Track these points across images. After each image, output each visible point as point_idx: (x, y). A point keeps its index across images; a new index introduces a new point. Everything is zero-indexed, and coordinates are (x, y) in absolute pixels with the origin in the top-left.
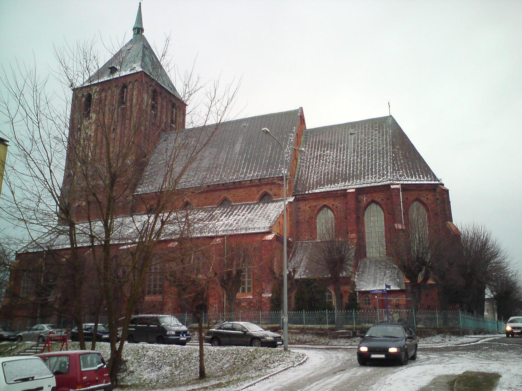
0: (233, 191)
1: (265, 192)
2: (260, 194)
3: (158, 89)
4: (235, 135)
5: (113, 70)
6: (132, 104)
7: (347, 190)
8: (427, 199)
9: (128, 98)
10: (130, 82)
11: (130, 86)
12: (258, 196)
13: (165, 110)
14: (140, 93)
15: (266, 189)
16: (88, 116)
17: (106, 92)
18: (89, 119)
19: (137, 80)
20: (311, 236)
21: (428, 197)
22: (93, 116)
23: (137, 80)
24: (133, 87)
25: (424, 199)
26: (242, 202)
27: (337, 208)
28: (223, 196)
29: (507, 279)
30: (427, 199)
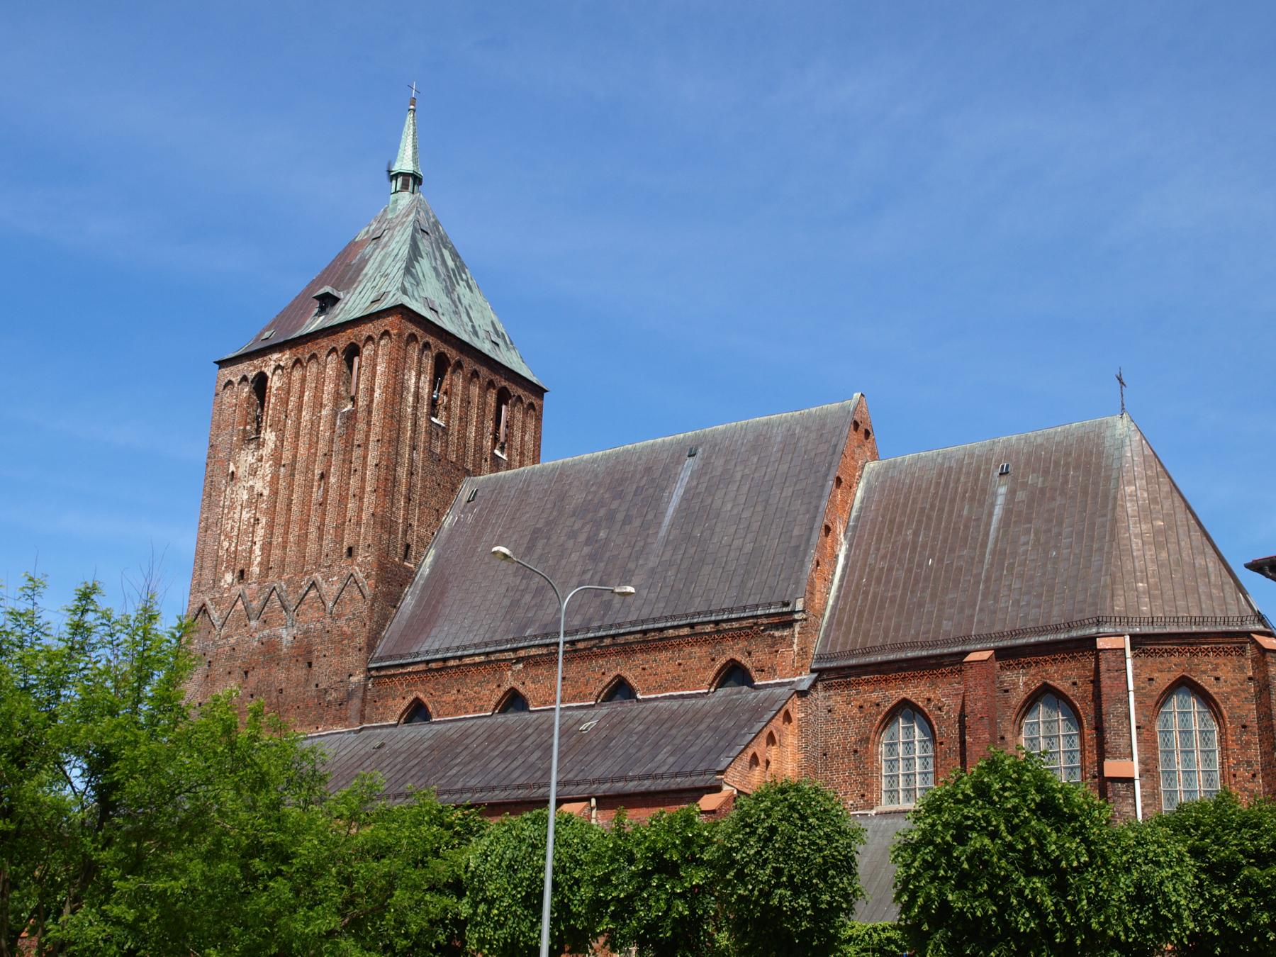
0: (640, 659)
1: (732, 660)
2: (718, 666)
3: (453, 355)
4: (278, 540)
5: (327, 302)
6: (372, 401)
7: (966, 653)
8: (1217, 679)
9: (361, 387)
10: (370, 338)
11: (367, 351)
12: (711, 675)
13: (474, 413)
14: (397, 370)
15: (734, 651)
16: (252, 439)
17: (304, 368)
18: (258, 448)
19: (386, 333)
20: (863, 796)
21: (1218, 674)
22: (269, 436)
23: (386, 333)
24: (376, 354)
25: (1205, 681)
26: (667, 690)
27: (940, 709)
28: (614, 673)
29: (834, 910)
30: (1217, 679)
